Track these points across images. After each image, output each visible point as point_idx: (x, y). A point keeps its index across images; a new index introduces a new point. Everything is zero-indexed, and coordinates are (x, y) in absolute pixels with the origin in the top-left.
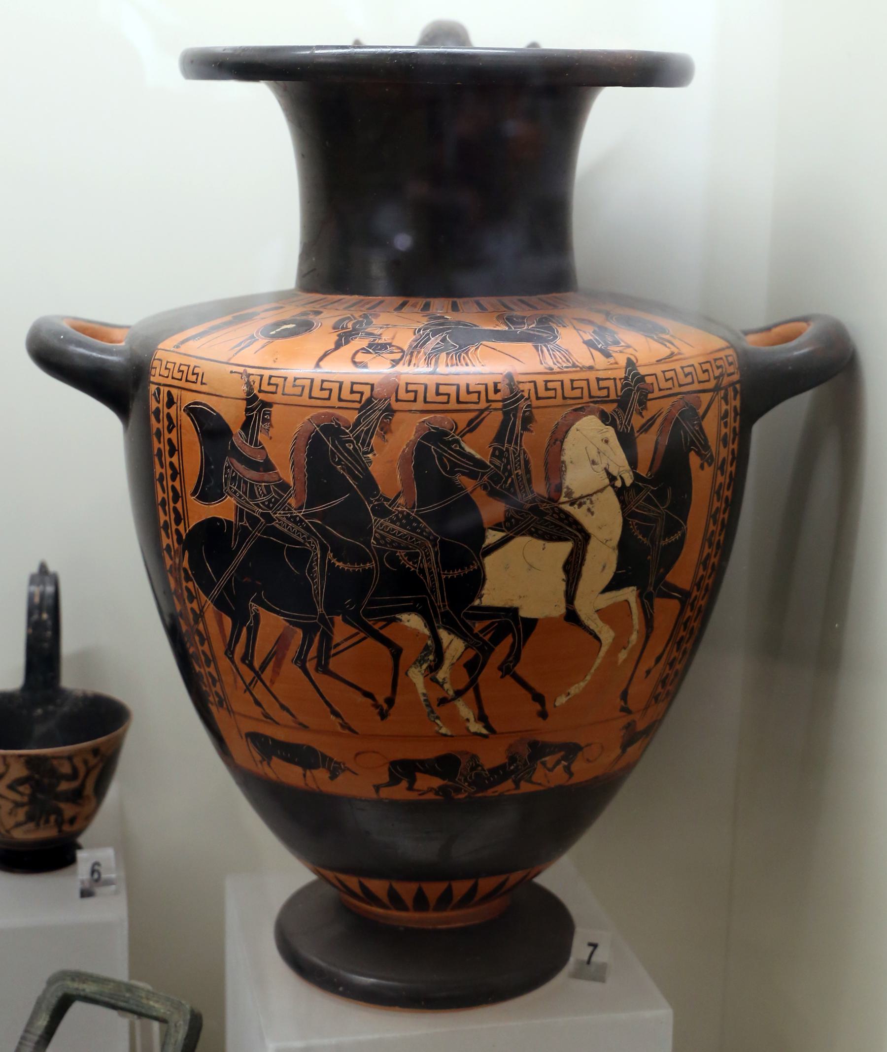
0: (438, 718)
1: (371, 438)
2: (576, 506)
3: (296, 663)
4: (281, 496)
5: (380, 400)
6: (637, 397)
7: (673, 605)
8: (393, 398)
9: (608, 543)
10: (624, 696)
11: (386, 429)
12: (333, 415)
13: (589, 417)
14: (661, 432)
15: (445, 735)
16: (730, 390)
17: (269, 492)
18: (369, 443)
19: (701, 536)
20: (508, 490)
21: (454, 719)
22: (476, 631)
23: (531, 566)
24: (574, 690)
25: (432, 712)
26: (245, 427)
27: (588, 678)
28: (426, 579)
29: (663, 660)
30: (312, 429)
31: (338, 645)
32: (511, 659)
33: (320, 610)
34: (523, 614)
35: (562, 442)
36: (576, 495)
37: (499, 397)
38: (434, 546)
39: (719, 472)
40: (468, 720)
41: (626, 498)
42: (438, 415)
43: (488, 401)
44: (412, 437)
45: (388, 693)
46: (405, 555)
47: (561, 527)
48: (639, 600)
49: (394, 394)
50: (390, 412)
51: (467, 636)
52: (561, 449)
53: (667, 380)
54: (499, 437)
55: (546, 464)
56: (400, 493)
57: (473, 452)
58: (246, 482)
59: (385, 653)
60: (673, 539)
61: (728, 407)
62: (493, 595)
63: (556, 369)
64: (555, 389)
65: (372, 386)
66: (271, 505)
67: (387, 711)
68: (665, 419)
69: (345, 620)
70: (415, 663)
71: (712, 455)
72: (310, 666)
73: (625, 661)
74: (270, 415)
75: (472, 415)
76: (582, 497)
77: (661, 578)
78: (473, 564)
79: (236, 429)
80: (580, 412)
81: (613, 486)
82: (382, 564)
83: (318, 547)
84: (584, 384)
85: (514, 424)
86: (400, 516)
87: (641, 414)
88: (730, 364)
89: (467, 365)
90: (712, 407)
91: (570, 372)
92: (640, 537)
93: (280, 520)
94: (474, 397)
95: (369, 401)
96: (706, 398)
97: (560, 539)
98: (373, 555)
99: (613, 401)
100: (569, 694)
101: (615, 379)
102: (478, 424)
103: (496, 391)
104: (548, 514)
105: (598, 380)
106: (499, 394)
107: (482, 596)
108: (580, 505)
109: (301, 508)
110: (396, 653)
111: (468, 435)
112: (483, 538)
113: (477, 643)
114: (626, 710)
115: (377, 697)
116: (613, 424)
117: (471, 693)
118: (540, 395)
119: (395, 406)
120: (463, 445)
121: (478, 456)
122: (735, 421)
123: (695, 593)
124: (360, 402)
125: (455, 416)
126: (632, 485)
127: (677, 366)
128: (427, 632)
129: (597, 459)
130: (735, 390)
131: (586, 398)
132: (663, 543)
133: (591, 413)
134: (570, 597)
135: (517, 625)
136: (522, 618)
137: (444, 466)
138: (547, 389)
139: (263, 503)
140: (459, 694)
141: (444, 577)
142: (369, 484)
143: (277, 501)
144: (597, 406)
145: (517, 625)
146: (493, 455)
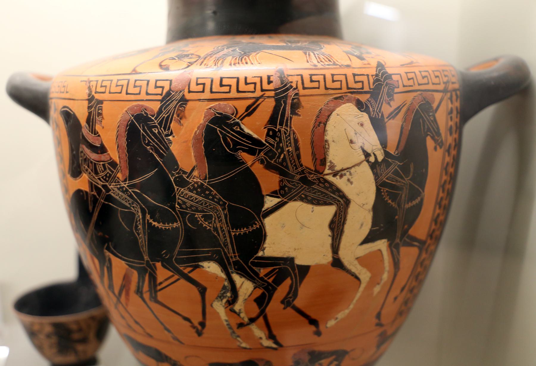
0: (238, 336)
1: (171, 123)
2: (338, 177)
3: (137, 294)
4: (113, 172)
5: (177, 92)
6: (386, 90)
7: (414, 251)
8: (186, 90)
9: (365, 206)
10: (378, 316)
11: (181, 117)
12: (142, 106)
13: (348, 104)
14: (405, 120)
15: (245, 348)
16: (454, 93)
17: (105, 169)
18: (169, 127)
19: (433, 201)
20: (281, 164)
21: (250, 337)
22: (262, 275)
23: (303, 225)
24: (341, 315)
25: (234, 332)
26: (88, 121)
27: (351, 306)
28: (219, 235)
29: (406, 289)
30: (128, 118)
31: (161, 283)
32: (290, 295)
33: (146, 258)
34: (298, 262)
35: (325, 125)
36: (338, 168)
37: (271, 87)
38: (224, 209)
39: (447, 154)
40: (261, 338)
41: (379, 171)
42: (222, 103)
43: (262, 90)
44: (202, 122)
45: (200, 319)
46: (202, 217)
47: (327, 194)
48: (389, 249)
49: (187, 87)
50: (184, 101)
51: (255, 279)
52: (324, 130)
53: (409, 79)
54: (272, 120)
55: (312, 142)
56: (194, 167)
57: (251, 133)
58: (91, 162)
59: (195, 291)
60: (414, 203)
61: (453, 106)
62: (272, 248)
63: (319, 66)
64: (319, 81)
65: (171, 81)
66: (107, 179)
67: (201, 331)
68: (408, 109)
69: (163, 266)
70: (217, 298)
71: (442, 141)
72: (146, 296)
73: (379, 293)
74: (101, 109)
75: (250, 102)
76: (343, 170)
77: (405, 232)
78: (256, 224)
79: (83, 122)
80: (339, 99)
81: (368, 161)
82: (185, 224)
83: (139, 211)
84: (343, 78)
85: (284, 109)
86: (196, 185)
87: (389, 104)
88: (453, 76)
89: (247, 63)
90: (442, 104)
91: (332, 68)
92: (390, 201)
93: (114, 190)
94: (251, 87)
95: (168, 94)
96: (438, 96)
97: (326, 204)
98: (178, 217)
99: (366, 92)
100: (337, 319)
101: (368, 75)
102: (255, 110)
103: (270, 82)
104: (315, 183)
105: (354, 75)
106: (271, 84)
107: (264, 249)
108: (341, 176)
109: (125, 180)
110: (203, 291)
111: (247, 118)
112: (262, 204)
113: (264, 284)
114: (379, 325)
115: (193, 321)
116: (367, 111)
117: (261, 320)
118: (305, 86)
119: (188, 96)
120: (243, 126)
121: (255, 136)
122: (457, 117)
123: (429, 241)
124: (161, 95)
125: (236, 103)
126: (383, 160)
127: (416, 70)
128: (223, 275)
129: (354, 139)
130: (456, 95)
131: (344, 89)
132: (407, 206)
133: (349, 101)
134: (335, 249)
135: (294, 270)
136: (298, 266)
137: (228, 145)
138: (312, 81)
139: (102, 177)
140: (252, 320)
141: (233, 234)
142: (172, 161)
143: (110, 175)
144: (353, 95)
145: (294, 270)
146: (268, 135)
